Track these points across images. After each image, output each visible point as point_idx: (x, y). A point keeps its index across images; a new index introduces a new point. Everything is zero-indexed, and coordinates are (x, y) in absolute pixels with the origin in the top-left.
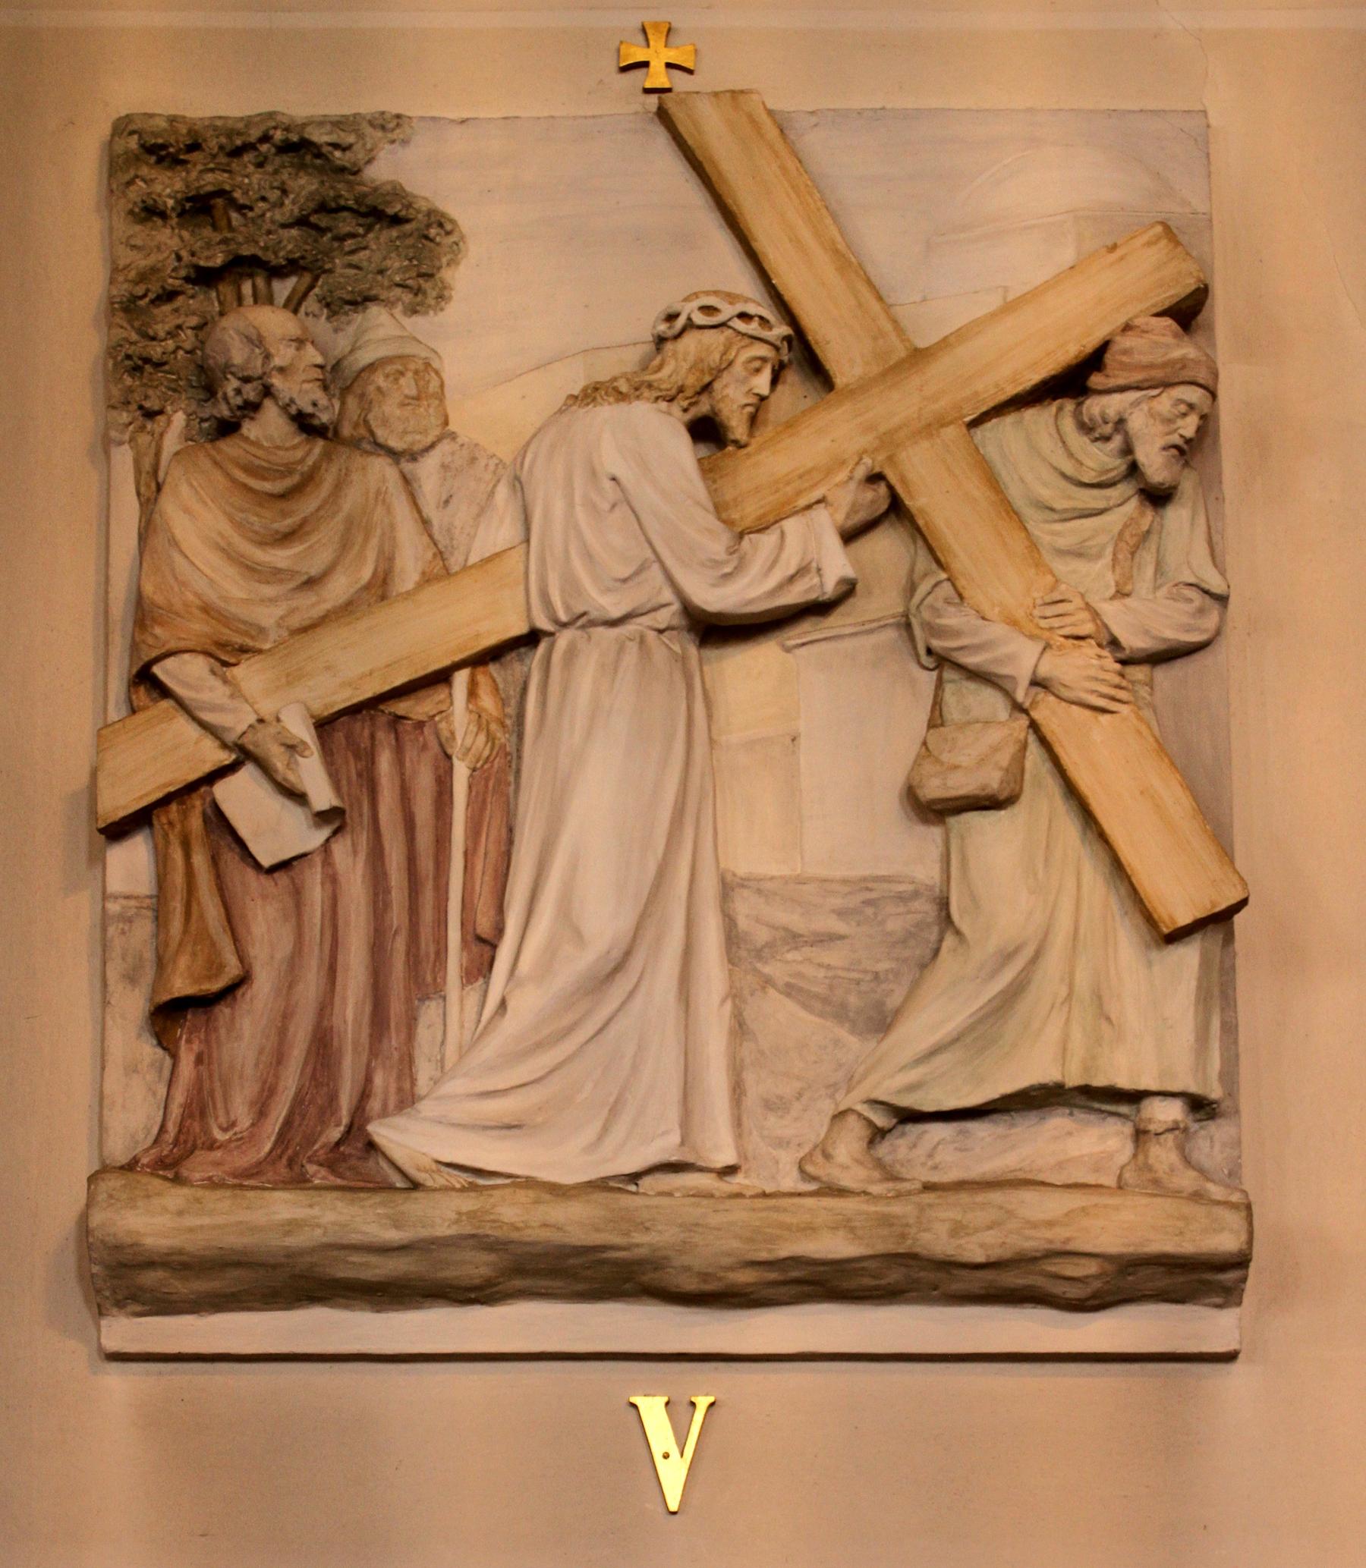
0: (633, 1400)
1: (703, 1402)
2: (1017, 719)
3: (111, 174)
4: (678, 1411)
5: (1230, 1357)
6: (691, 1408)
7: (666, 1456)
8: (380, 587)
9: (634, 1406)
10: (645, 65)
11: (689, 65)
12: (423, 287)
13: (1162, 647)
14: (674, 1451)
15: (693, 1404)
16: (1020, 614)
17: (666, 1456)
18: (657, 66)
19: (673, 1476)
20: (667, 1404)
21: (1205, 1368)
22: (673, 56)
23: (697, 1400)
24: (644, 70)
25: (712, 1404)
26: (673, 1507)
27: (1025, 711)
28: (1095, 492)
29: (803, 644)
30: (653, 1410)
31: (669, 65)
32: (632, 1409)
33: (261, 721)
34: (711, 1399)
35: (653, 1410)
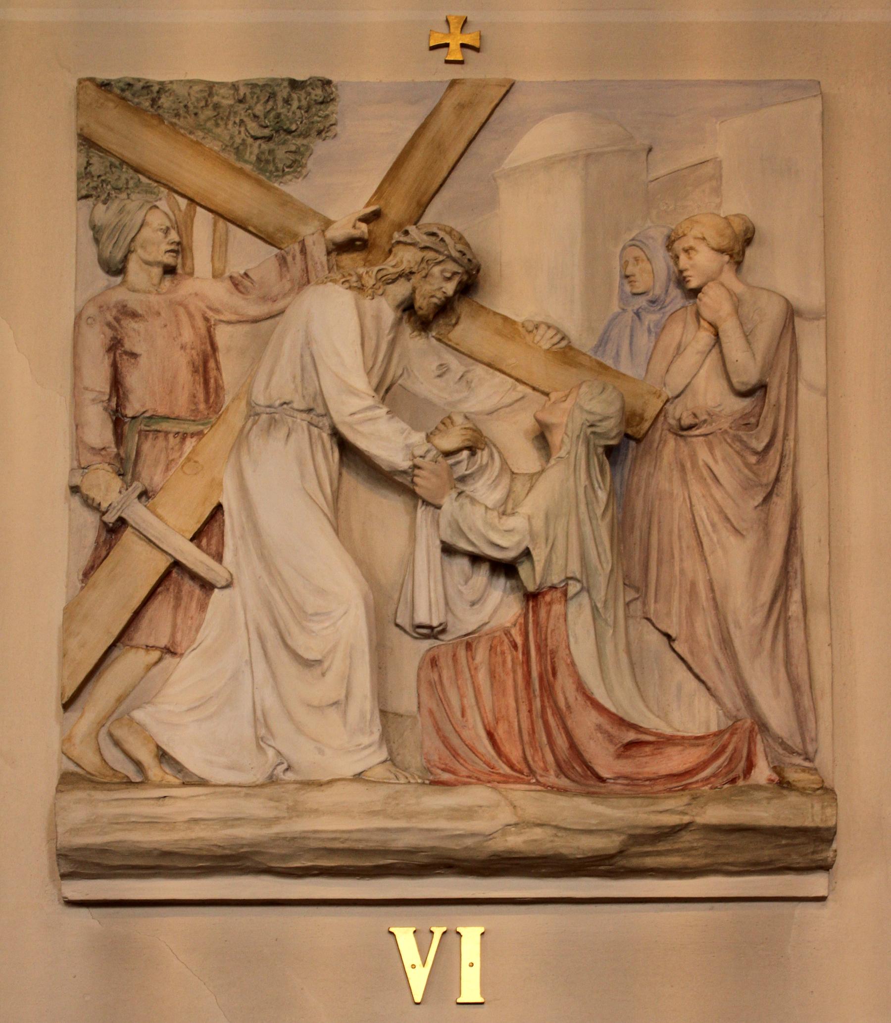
0: (392, 930)
1: (438, 931)
4: (422, 939)
5: (822, 899)
6: (430, 934)
10: (447, 45)
11: (477, 45)
13: (749, 387)
14: (418, 961)
15: (432, 932)
16: (584, 342)
17: (472, 965)
18: (454, 45)
19: (418, 979)
21: (801, 905)
22: (467, 40)
24: (446, 49)
25: (444, 933)
26: (418, 999)
28: (672, 311)
29: (430, 610)
30: (405, 938)
31: (463, 46)
32: (391, 936)
33: (694, 293)
34: (444, 929)
35: (405, 938)
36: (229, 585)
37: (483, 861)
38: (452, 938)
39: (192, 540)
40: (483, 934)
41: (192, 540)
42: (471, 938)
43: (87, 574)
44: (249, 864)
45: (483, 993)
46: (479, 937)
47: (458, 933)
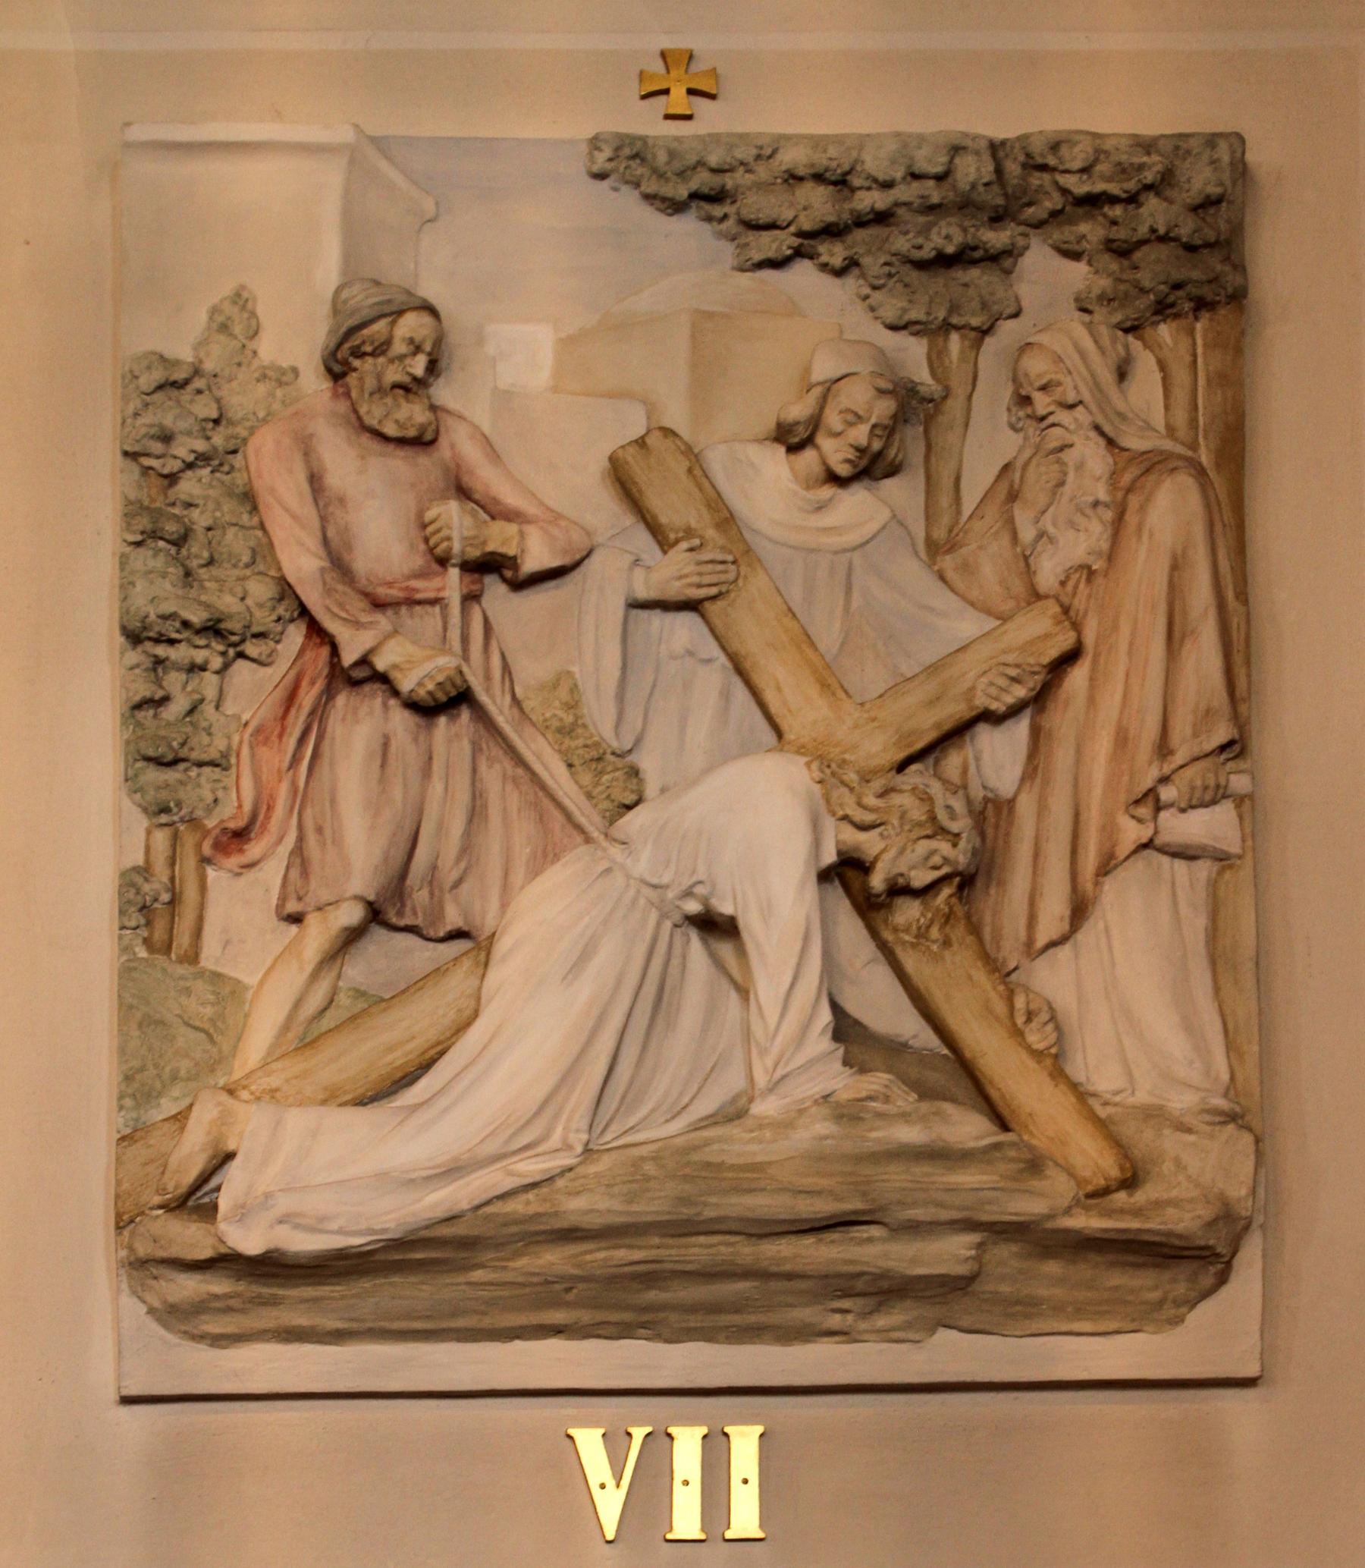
0: (571, 1431)
1: (639, 1433)
2: (459, 715)
3: (1237, 229)
4: (615, 1443)
6: (627, 1438)
7: (603, 1486)
8: (158, 788)
9: (726, 1435)
12: (1079, 293)
14: (611, 1483)
15: (629, 1434)
17: (686, 1483)
19: (610, 1505)
20: (604, 1435)
23: (633, 1430)
26: (610, 1536)
27: (426, 710)
30: (590, 1443)
31: (691, 92)
32: (568, 1440)
34: (649, 1429)
35: (590, 1443)
36: (1016, 315)
37: (1052, 1258)
38: (660, 1442)
39: (665, 552)
40: (705, 1437)
41: (665, 552)
42: (745, 1445)
43: (588, 556)
44: (995, 1208)
45: (703, 1530)
46: (700, 1442)
47: (669, 1435)
